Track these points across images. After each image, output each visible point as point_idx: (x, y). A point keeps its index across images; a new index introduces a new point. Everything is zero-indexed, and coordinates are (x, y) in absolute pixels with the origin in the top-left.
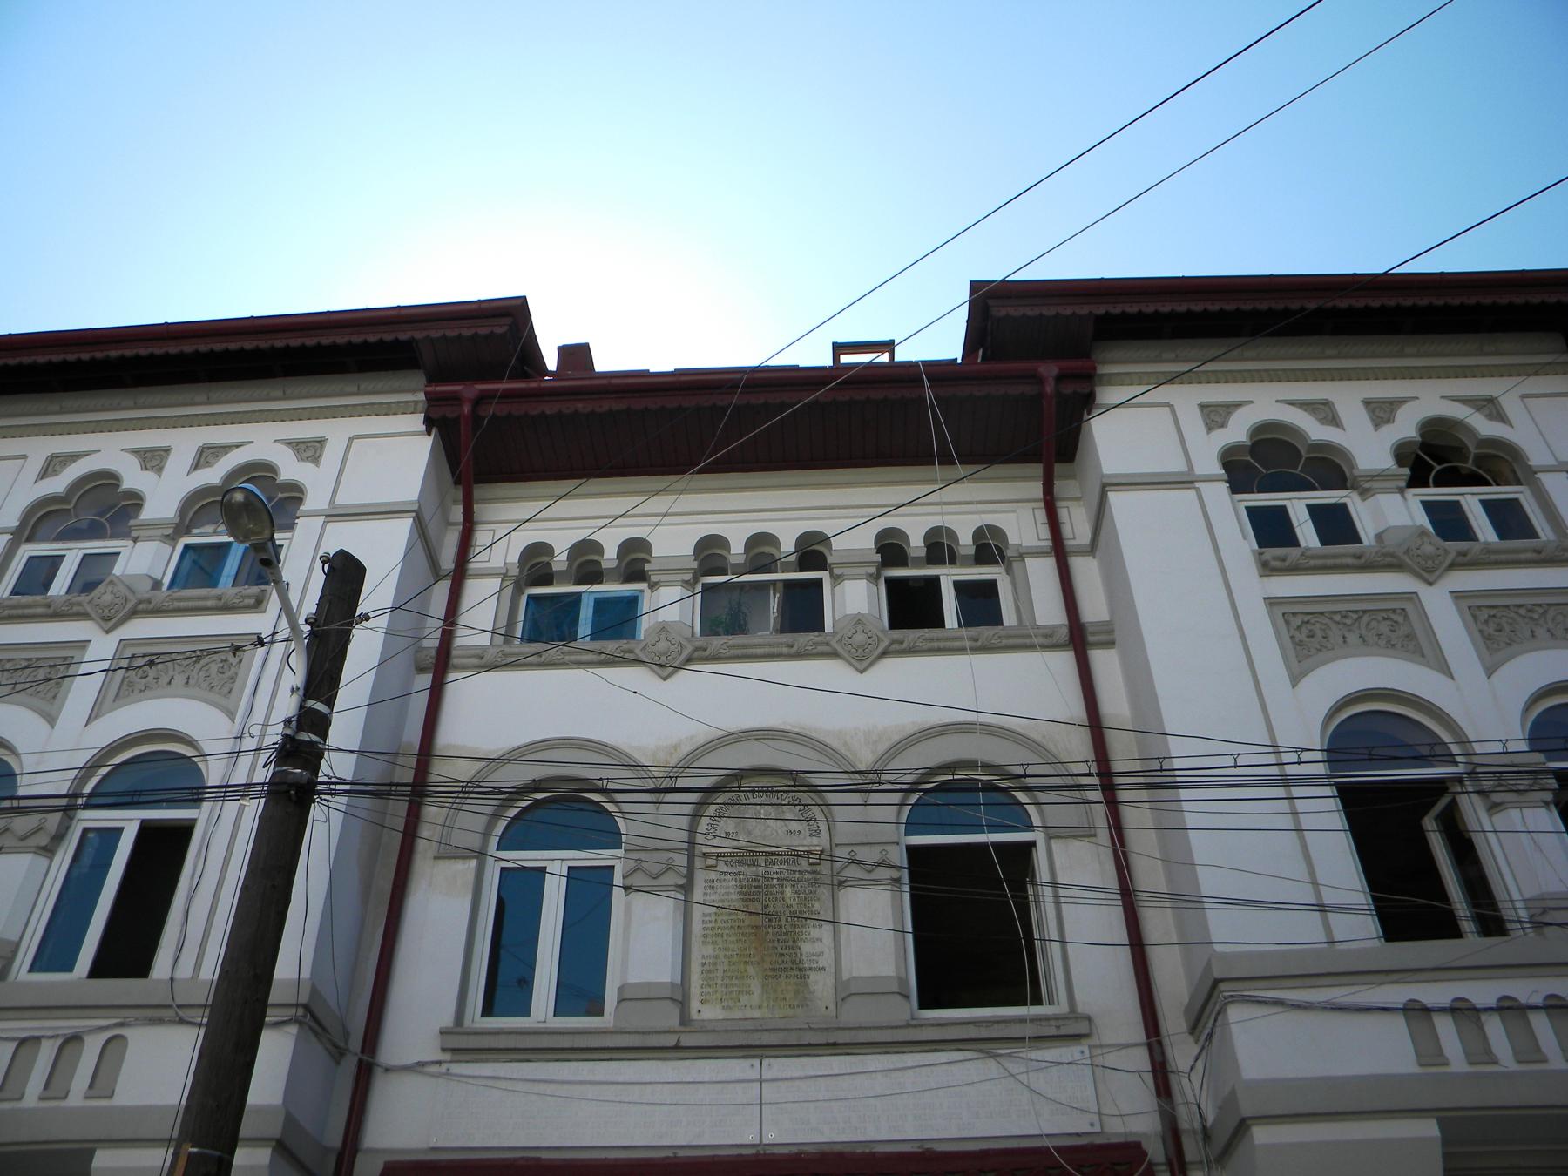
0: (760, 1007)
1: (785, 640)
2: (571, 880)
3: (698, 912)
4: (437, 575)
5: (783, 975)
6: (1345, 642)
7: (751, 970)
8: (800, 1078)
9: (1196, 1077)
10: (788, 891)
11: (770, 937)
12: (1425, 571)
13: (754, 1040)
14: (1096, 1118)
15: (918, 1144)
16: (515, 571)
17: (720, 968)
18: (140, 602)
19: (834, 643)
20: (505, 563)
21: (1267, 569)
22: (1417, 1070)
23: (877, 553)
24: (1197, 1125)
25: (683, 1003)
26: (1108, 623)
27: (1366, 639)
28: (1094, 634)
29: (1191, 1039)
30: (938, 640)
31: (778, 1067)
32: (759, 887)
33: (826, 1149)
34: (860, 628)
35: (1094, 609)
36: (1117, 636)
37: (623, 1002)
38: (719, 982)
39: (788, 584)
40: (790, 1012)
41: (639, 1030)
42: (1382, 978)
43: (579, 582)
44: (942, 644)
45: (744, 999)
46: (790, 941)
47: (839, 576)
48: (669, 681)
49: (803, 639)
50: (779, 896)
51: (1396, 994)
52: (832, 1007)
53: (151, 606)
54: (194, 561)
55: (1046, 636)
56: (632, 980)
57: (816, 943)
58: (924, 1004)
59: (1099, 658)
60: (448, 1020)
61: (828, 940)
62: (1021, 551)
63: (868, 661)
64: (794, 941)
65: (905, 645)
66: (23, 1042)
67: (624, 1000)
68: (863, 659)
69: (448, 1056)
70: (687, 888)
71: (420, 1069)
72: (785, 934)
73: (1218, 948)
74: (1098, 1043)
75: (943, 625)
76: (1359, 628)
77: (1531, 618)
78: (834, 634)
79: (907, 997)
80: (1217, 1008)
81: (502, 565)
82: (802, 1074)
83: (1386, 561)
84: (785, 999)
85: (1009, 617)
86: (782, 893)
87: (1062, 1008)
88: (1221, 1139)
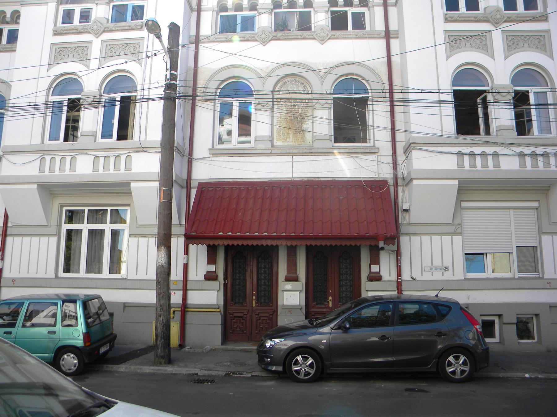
0: (292, 142)
1: (299, 34)
2: (240, 107)
3: (275, 115)
4: (192, 10)
5: (298, 133)
6: (465, 46)
7: (290, 132)
8: (302, 161)
9: (403, 166)
10: (300, 110)
11: (295, 123)
12: (495, 23)
13: (291, 151)
14: (377, 174)
15: (332, 178)
16: (216, 9)
17: (282, 131)
18: (105, 28)
19: (314, 36)
20: (213, 6)
21: (447, 20)
22: (457, 168)
23: (328, 3)
24: (402, 176)
25: (272, 141)
26: (398, 30)
27: (472, 45)
28: (392, 34)
29: (404, 155)
30: (346, 35)
31: (296, 158)
32: (292, 109)
33: (309, 179)
34: (322, 31)
35: (393, 26)
36: (399, 36)
37: (256, 141)
38: (281, 135)
39: (300, 12)
40: (300, 143)
41: (261, 149)
42: (453, 145)
43: (236, 11)
44: (346, 36)
45: (288, 140)
46: (301, 122)
47: (316, 11)
48: (265, 46)
49: (306, 33)
50: (297, 111)
51: (456, 149)
52: (311, 142)
53: (109, 29)
54: (116, 10)
55: (378, 35)
56: (258, 135)
57: (307, 125)
58: (335, 142)
59: (393, 42)
60: (210, 146)
61: (311, 124)
62: (373, 4)
63: (324, 41)
64: (301, 124)
65: (335, 36)
66: (105, 157)
67: (256, 140)
68: (322, 41)
69: (211, 156)
70: (272, 109)
71: (204, 159)
72: (299, 122)
73: (413, 135)
74: (379, 155)
75: (347, 30)
76: (471, 41)
77: (525, 40)
78: (315, 32)
79: (331, 140)
80: (410, 150)
81: (212, 7)
82: (303, 160)
83: (485, 20)
84: (299, 140)
85: (368, 27)
86: (298, 110)
87: (371, 144)
88: (407, 181)
